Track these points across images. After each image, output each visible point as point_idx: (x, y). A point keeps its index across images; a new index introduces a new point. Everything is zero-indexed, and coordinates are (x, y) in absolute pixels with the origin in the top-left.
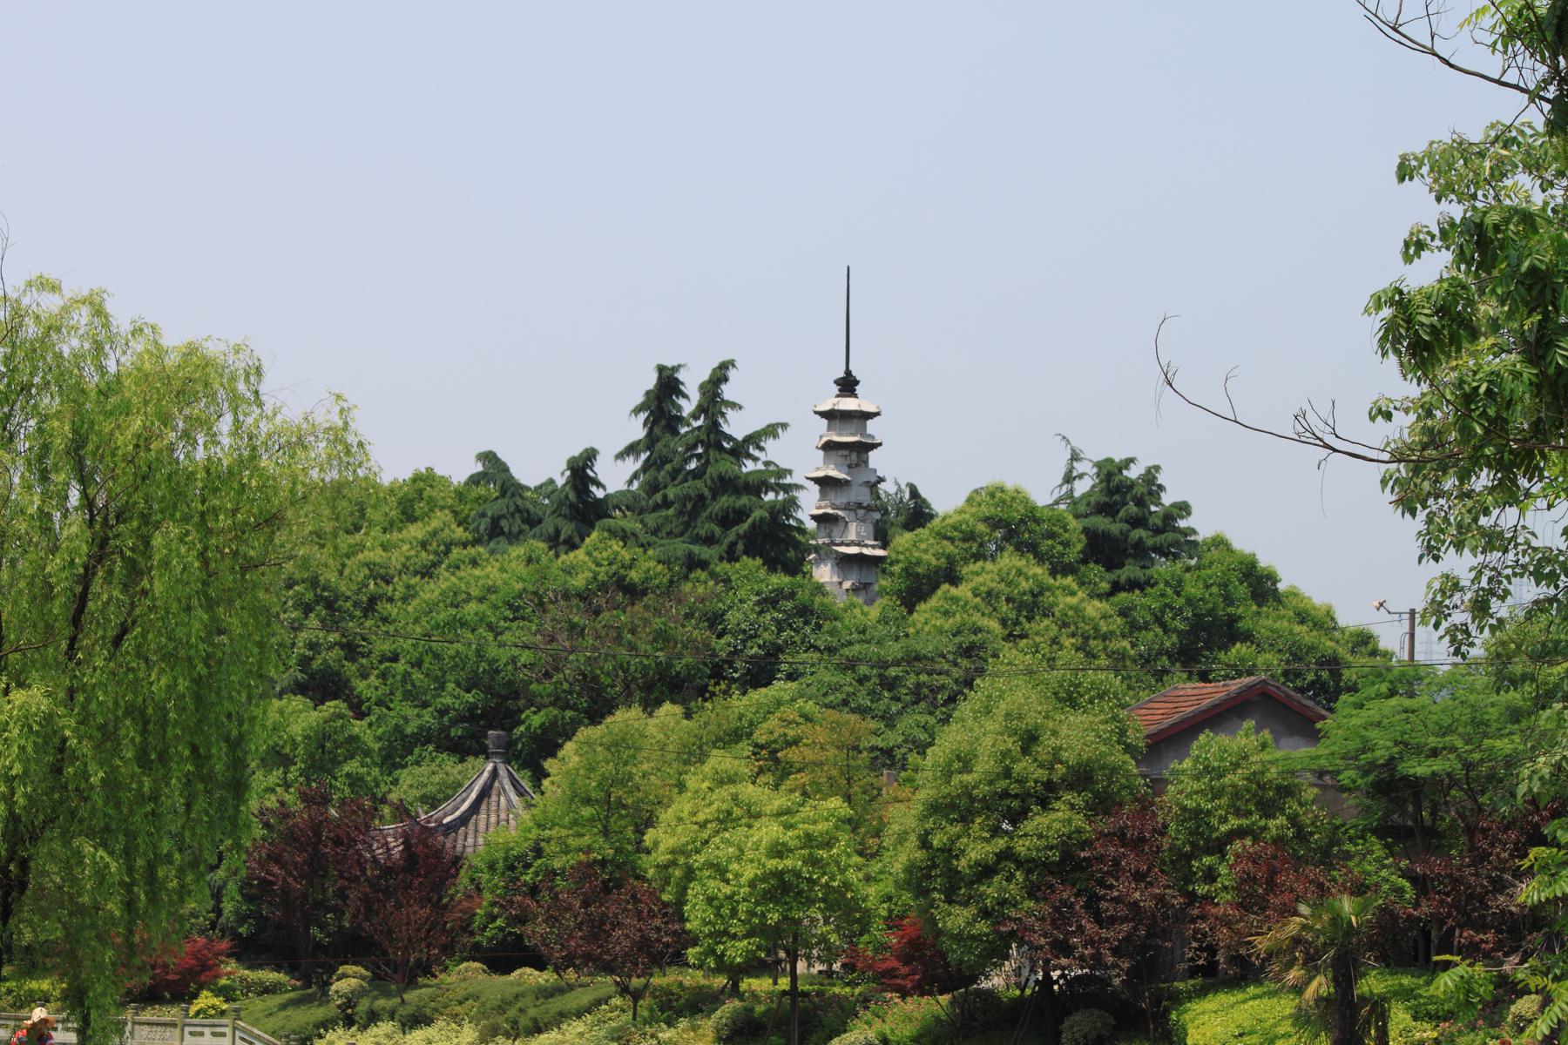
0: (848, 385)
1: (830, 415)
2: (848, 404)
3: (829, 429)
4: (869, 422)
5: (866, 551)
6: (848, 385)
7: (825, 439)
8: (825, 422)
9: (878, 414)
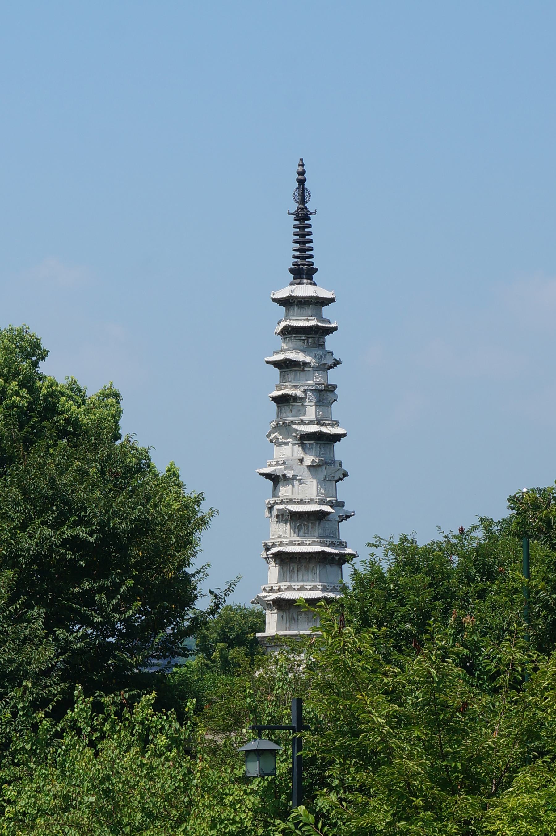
0: (303, 271)
1: (288, 303)
2: (305, 290)
3: (287, 315)
4: (325, 308)
5: (324, 430)
6: (303, 271)
7: (283, 324)
8: (283, 309)
9: (332, 300)
